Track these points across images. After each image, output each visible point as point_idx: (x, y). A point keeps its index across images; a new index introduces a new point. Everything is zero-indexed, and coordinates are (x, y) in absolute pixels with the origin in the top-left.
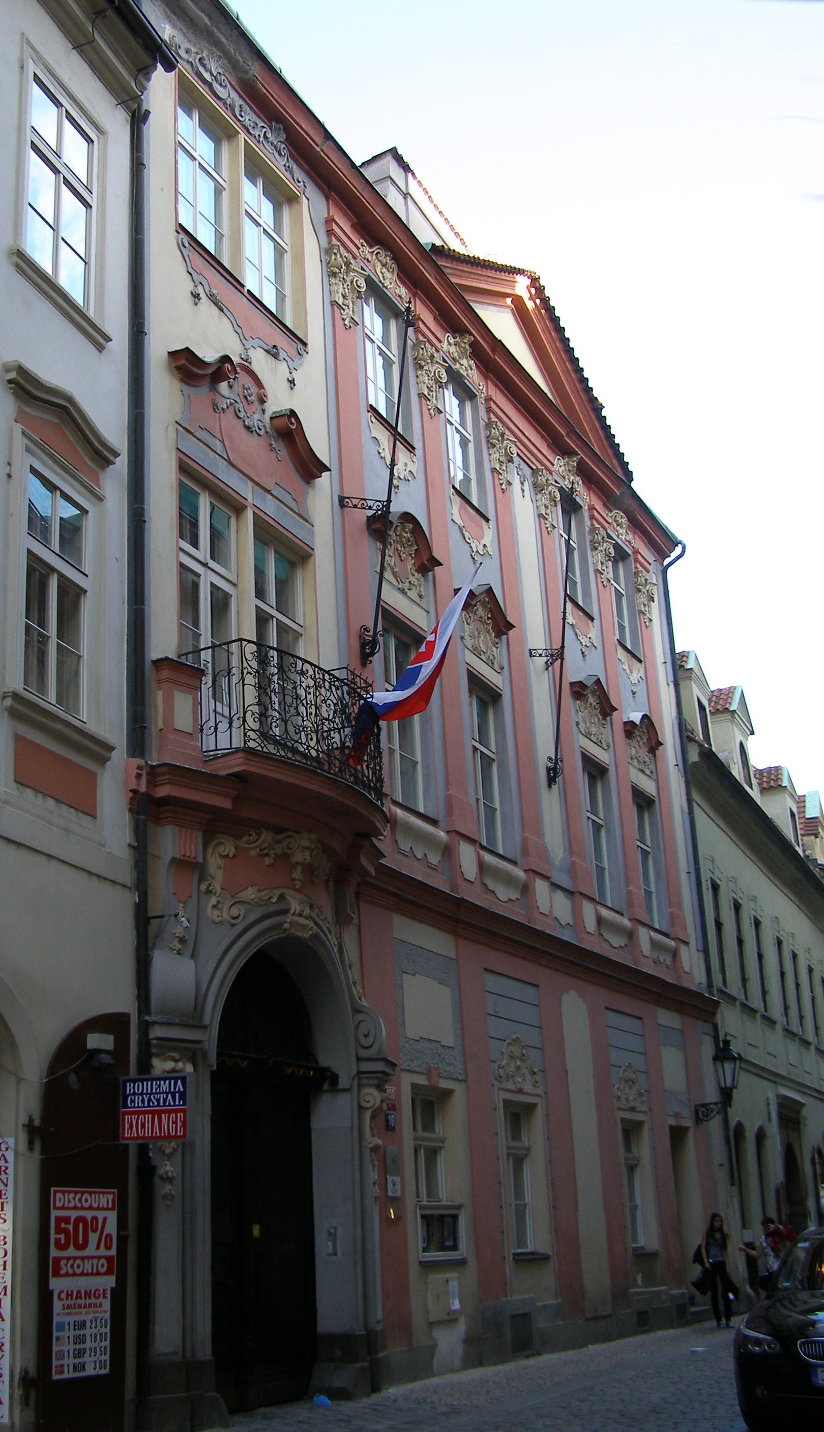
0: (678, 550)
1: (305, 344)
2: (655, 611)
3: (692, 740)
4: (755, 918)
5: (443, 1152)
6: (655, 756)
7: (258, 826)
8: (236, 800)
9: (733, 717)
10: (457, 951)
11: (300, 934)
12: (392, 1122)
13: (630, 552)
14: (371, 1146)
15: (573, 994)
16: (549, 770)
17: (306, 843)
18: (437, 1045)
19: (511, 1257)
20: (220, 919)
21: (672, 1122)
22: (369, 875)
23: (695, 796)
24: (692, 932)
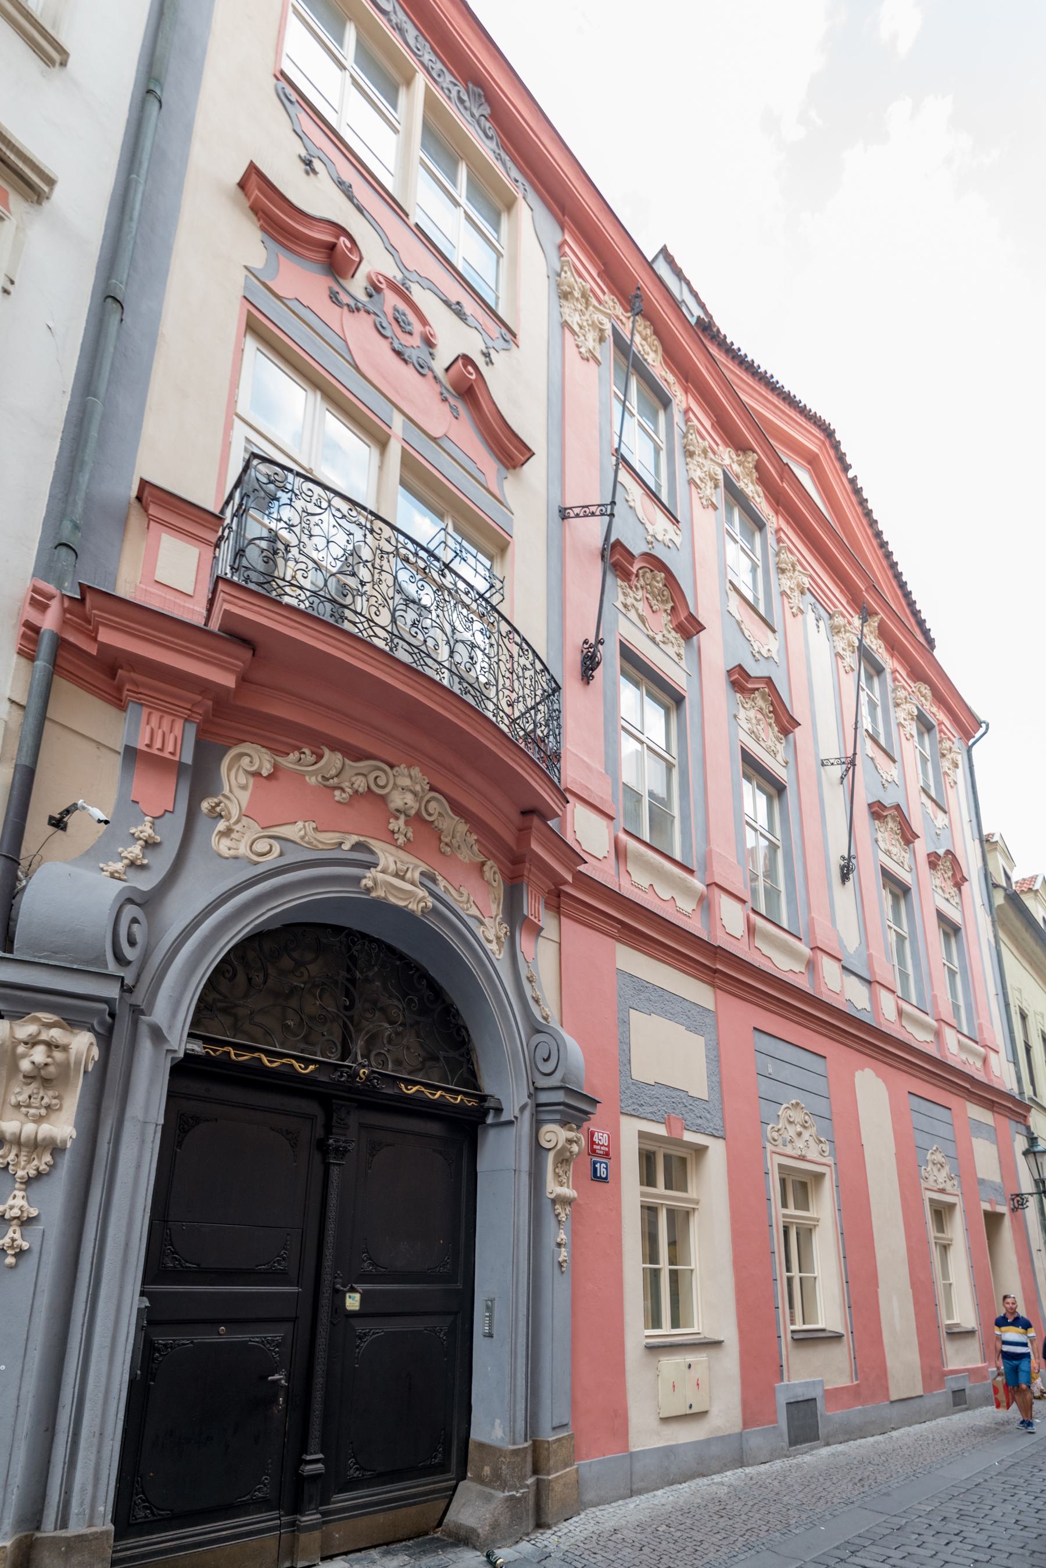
0: (982, 730)
1: (514, 335)
2: (960, 775)
3: (996, 886)
4: (1020, 1008)
5: (696, 1213)
6: (960, 890)
7: (319, 742)
8: (243, 679)
9: (1036, 895)
11: (402, 904)
12: (602, 1171)
13: (935, 723)
14: (552, 1196)
15: (869, 1073)
16: (842, 868)
17: (406, 782)
18: (682, 1094)
19: (789, 1335)
20: (232, 852)
21: (986, 1206)
22: (566, 882)
23: (1002, 935)
24: (999, 1039)
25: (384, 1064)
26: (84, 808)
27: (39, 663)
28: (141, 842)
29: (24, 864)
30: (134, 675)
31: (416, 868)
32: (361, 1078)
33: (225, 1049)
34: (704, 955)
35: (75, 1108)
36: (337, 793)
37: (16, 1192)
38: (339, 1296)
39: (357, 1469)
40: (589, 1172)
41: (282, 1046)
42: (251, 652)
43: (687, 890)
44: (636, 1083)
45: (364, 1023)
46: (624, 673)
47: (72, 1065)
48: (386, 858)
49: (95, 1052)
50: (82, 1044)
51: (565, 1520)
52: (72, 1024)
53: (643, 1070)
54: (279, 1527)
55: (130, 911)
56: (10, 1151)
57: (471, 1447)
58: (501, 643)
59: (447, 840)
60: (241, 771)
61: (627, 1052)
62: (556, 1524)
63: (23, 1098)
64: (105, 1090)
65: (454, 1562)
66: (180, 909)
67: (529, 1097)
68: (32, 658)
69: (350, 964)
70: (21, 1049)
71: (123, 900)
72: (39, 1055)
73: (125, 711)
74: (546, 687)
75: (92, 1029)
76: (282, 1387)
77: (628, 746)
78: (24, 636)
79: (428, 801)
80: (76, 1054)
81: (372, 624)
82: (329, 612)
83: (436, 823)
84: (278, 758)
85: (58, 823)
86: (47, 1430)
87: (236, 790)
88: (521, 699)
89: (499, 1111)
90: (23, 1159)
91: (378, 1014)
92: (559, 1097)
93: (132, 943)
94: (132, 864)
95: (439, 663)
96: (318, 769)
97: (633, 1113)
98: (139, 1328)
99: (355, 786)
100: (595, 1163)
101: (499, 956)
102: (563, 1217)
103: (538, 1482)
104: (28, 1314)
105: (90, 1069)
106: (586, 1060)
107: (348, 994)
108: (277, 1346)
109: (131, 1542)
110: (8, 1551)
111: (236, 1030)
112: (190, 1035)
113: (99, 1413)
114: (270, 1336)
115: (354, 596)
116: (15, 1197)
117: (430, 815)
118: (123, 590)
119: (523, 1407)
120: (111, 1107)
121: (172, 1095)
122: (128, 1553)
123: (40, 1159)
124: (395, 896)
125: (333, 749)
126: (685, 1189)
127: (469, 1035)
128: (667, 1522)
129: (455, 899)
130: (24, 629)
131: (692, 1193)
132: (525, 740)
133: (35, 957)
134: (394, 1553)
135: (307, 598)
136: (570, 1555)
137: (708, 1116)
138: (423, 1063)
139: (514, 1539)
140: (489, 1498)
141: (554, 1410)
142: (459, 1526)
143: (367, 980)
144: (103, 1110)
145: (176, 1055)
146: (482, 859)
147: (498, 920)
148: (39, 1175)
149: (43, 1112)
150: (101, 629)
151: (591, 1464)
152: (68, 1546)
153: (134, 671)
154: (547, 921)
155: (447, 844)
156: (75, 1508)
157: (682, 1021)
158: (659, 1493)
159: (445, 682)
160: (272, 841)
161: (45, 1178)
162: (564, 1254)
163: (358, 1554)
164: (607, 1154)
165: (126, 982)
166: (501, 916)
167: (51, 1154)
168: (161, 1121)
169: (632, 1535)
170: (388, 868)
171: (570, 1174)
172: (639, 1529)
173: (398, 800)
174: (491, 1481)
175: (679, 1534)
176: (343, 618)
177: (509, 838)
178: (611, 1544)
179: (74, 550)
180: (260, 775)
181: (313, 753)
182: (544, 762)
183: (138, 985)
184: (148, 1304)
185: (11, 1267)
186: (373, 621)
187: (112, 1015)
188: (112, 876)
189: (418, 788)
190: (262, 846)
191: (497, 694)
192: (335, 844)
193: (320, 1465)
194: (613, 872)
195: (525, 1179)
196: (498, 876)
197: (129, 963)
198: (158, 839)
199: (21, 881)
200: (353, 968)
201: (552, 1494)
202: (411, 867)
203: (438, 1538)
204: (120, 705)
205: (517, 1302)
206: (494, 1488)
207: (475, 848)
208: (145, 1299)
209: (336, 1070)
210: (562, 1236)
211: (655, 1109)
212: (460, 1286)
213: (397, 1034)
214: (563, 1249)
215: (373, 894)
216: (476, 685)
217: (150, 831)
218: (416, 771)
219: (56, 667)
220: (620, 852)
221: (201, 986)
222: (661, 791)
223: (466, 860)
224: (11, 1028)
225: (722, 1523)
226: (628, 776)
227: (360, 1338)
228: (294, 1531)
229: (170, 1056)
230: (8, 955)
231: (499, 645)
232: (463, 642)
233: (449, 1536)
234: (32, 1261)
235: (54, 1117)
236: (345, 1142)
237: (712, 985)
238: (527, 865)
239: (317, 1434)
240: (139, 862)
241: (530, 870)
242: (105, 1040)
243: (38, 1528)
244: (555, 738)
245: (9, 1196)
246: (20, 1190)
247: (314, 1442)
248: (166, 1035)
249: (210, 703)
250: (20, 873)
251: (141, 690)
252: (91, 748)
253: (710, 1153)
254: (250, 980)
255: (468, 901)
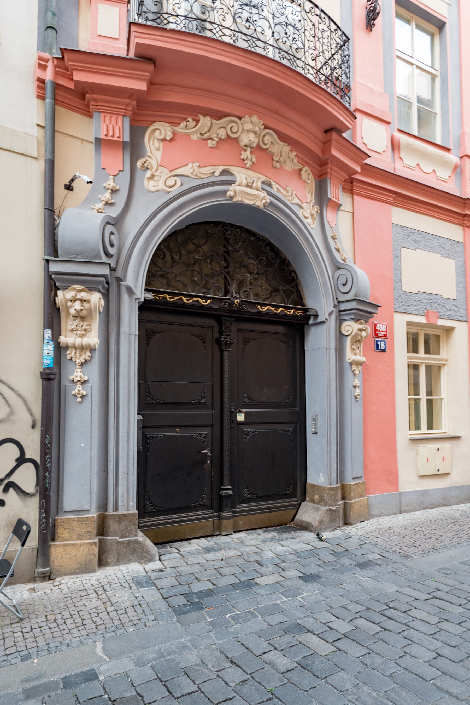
5: (446, 367)
7: (195, 112)
8: (151, 84)
10: (464, 237)
11: (251, 203)
14: (350, 361)
17: (249, 126)
18: (437, 297)
20: (156, 188)
22: (356, 172)
25: (248, 296)
26: (80, 177)
27: (48, 100)
28: (110, 191)
29: (57, 211)
30: (94, 96)
31: (258, 179)
32: (236, 305)
33: (164, 296)
34: (458, 206)
35: (97, 330)
36: (209, 142)
37: (77, 370)
38: (233, 415)
39: (249, 494)
40: (374, 347)
41: (193, 291)
42: (153, 65)
43: (444, 163)
44: (405, 293)
45: (236, 275)
46: (398, 15)
47: (93, 309)
48: (240, 176)
49: (103, 302)
50: (96, 298)
51: (361, 522)
52: (90, 290)
53: (410, 284)
54: (213, 517)
55: (109, 229)
56: (72, 351)
57: (307, 486)
58: (306, 17)
59: (277, 159)
60: (156, 140)
61: (399, 275)
62: (355, 523)
63: (74, 327)
64: (110, 319)
65: (300, 537)
66: (132, 225)
67: (334, 307)
68: (43, 99)
69: (226, 243)
70: (69, 304)
71: (104, 223)
72: (77, 306)
73: (92, 118)
74: (339, 41)
75: (99, 291)
76: (209, 456)
77: (402, 70)
78: (38, 87)
79: (264, 136)
80: (94, 304)
81: (221, 27)
82: (195, 27)
83: (270, 149)
84: (175, 128)
85: (69, 187)
86: (104, 471)
87: (154, 152)
88: (321, 54)
89: (316, 316)
90: (78, 354)
91: (243, 269)
92: (353, 305)
93: (112, 245)
94: (107, 203)
95: (265, 43)
96: (198, 129)
97: (403, 311)
98: (139, 429)
99: (220, 135)
100: (377, 341)
101: (313, 226)
102: (357, 372)
103: (345, 504)
104: (90, 422)
105: (101, 311)
106: (371, 283)
107: (225, 260)
108: (205, 437)
109: (146, 519)
110: (95, 518)
111: (169, 285)
112: (146, 290)
113: (126, 464)
114: (201, 433)
115: (209, 12)
116: (77, 372)
117: (265, 144)
118: (83, 47)
119: (335, 467)
120: (113, 327)
121: (141, 321)
122: (146, 524)
123: (85, 354)
124: (248, 199)
125: (205, 115)
126: (439, 354)
127: (296, 275)
128: (421, 526)
129: (284, 195)
130: (37, 83)
131: (443, 354)
132: (326, 83)
133: (69, 258)
134: (270, 532)
135: (181, 21)
136: (362, 537)
137: (456, 309)
138: (271, 293)
139: (332, 529)
140: (318, 510)
141: (353, 470)
142: (303, 522)
143: (236, 251)
144: (110, 330)
145: (140, 301)
146: (300, 166)
147: (312, 203)
148: (86, 361)
149: (83, 332)
150: (75, 73)
151: (376, 497)
152: (119, 518)
153: (94, 93)
154: (344, 200)
155: (277, 161)
156: (120, 503)
157: (439, 251)
158: (418, 513)
159: (270, 55)
160: (176, 178)
161: (89, 363)
162: (358, 391)
163: (252, 531)
164: (385, 336)
165: (112, 266)
166: (313, 201)
167: (90, 352)
168: (137, 333)
169: (399, 531)
170: (242, 183)
171: (361, 348)
172: (404, 528)
173: (245, 139)
174: (319, 502)
175: (428, 531)
176: (204, 29)
177: (317, 150)
178: (386, 534)
179: (56, 30)
180: (166, 140)
181: (194, 120)
182: (338, 94)
183: (118, 267)
184: (142, 418)
185: (80, 403)
186: (222, 26)
187: (108, 283)
188: (98, 212)
189: (257, 129)
190: (171, 182)
191: (305, 54)
192: (211, 173)
193: (230, 491)
194: (390, 160)
195: (333, 353)
196: (311, 176)
197: (112, 256)
198: (118, 187)
199: (56, 220)
200: (227, 245)
201: (353, 509)
202: (256, 179)
203: (292, 527)
204: (90, 115)
205: (330, 416)
206: (320, 505)
207: (295, 160)
208: (140, 416)
209: (222, 302)
210: (357, 382)
211: (418, 307)
212: (298, 409)
213: (255, 279)
214: (357, 389)
215: (235, 200)
216: (290, 52)
217: (113, 184)
218: (255, 118)
219: (56, 101)
220: (395, 146)
221: (148, 264)
222: (426, 95)
223: (290, 169)
224: (64, 294)
225: (455, 528)
226: (401, 89)
227: (246, 435)
228: (220, 519)
229: (137, 301)
230: (56, 259)
231: (304, 19)
232: (280, 24)
233: (298, 526)
234: (88, 399)
235: (88, 334)
236: (230, 339)
237: (462, 225)
238: (330, 166)
239: (228, 477)
240: (110, 202)
241: (331, 169)
242: (106, 296)
243: (106, 511)
244: (346, 76)
245: (74, 371)
246: (79, 369)
247: (226, 481)
248: (134, 291)
249: (134, 103)
250: (55, 217)
251: (99, 104)
252: (78, 142)
253: (456, 331)
254: (172, 258)
255: (292, 195)
